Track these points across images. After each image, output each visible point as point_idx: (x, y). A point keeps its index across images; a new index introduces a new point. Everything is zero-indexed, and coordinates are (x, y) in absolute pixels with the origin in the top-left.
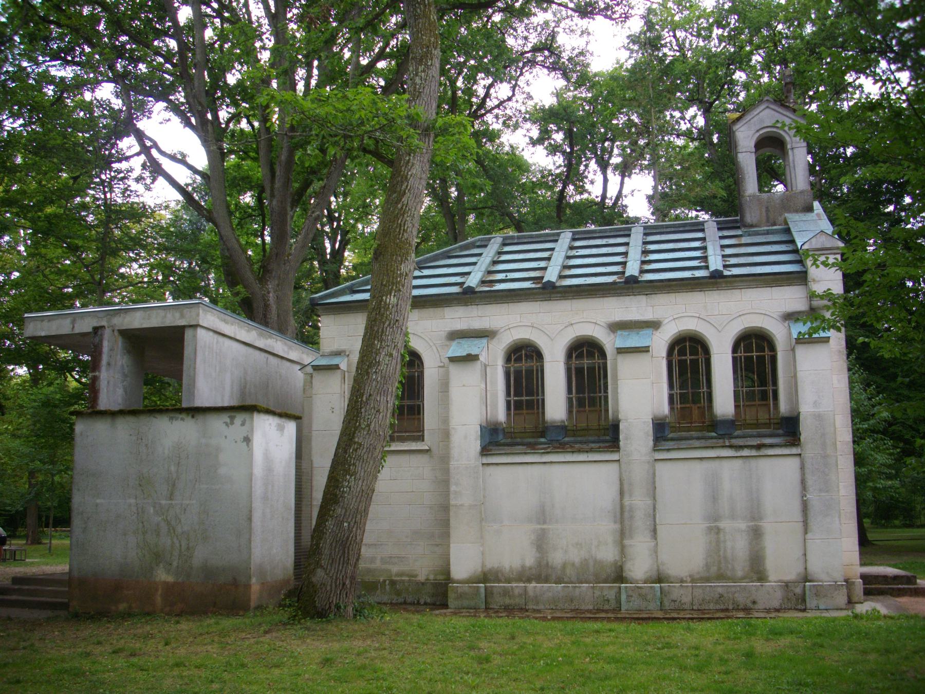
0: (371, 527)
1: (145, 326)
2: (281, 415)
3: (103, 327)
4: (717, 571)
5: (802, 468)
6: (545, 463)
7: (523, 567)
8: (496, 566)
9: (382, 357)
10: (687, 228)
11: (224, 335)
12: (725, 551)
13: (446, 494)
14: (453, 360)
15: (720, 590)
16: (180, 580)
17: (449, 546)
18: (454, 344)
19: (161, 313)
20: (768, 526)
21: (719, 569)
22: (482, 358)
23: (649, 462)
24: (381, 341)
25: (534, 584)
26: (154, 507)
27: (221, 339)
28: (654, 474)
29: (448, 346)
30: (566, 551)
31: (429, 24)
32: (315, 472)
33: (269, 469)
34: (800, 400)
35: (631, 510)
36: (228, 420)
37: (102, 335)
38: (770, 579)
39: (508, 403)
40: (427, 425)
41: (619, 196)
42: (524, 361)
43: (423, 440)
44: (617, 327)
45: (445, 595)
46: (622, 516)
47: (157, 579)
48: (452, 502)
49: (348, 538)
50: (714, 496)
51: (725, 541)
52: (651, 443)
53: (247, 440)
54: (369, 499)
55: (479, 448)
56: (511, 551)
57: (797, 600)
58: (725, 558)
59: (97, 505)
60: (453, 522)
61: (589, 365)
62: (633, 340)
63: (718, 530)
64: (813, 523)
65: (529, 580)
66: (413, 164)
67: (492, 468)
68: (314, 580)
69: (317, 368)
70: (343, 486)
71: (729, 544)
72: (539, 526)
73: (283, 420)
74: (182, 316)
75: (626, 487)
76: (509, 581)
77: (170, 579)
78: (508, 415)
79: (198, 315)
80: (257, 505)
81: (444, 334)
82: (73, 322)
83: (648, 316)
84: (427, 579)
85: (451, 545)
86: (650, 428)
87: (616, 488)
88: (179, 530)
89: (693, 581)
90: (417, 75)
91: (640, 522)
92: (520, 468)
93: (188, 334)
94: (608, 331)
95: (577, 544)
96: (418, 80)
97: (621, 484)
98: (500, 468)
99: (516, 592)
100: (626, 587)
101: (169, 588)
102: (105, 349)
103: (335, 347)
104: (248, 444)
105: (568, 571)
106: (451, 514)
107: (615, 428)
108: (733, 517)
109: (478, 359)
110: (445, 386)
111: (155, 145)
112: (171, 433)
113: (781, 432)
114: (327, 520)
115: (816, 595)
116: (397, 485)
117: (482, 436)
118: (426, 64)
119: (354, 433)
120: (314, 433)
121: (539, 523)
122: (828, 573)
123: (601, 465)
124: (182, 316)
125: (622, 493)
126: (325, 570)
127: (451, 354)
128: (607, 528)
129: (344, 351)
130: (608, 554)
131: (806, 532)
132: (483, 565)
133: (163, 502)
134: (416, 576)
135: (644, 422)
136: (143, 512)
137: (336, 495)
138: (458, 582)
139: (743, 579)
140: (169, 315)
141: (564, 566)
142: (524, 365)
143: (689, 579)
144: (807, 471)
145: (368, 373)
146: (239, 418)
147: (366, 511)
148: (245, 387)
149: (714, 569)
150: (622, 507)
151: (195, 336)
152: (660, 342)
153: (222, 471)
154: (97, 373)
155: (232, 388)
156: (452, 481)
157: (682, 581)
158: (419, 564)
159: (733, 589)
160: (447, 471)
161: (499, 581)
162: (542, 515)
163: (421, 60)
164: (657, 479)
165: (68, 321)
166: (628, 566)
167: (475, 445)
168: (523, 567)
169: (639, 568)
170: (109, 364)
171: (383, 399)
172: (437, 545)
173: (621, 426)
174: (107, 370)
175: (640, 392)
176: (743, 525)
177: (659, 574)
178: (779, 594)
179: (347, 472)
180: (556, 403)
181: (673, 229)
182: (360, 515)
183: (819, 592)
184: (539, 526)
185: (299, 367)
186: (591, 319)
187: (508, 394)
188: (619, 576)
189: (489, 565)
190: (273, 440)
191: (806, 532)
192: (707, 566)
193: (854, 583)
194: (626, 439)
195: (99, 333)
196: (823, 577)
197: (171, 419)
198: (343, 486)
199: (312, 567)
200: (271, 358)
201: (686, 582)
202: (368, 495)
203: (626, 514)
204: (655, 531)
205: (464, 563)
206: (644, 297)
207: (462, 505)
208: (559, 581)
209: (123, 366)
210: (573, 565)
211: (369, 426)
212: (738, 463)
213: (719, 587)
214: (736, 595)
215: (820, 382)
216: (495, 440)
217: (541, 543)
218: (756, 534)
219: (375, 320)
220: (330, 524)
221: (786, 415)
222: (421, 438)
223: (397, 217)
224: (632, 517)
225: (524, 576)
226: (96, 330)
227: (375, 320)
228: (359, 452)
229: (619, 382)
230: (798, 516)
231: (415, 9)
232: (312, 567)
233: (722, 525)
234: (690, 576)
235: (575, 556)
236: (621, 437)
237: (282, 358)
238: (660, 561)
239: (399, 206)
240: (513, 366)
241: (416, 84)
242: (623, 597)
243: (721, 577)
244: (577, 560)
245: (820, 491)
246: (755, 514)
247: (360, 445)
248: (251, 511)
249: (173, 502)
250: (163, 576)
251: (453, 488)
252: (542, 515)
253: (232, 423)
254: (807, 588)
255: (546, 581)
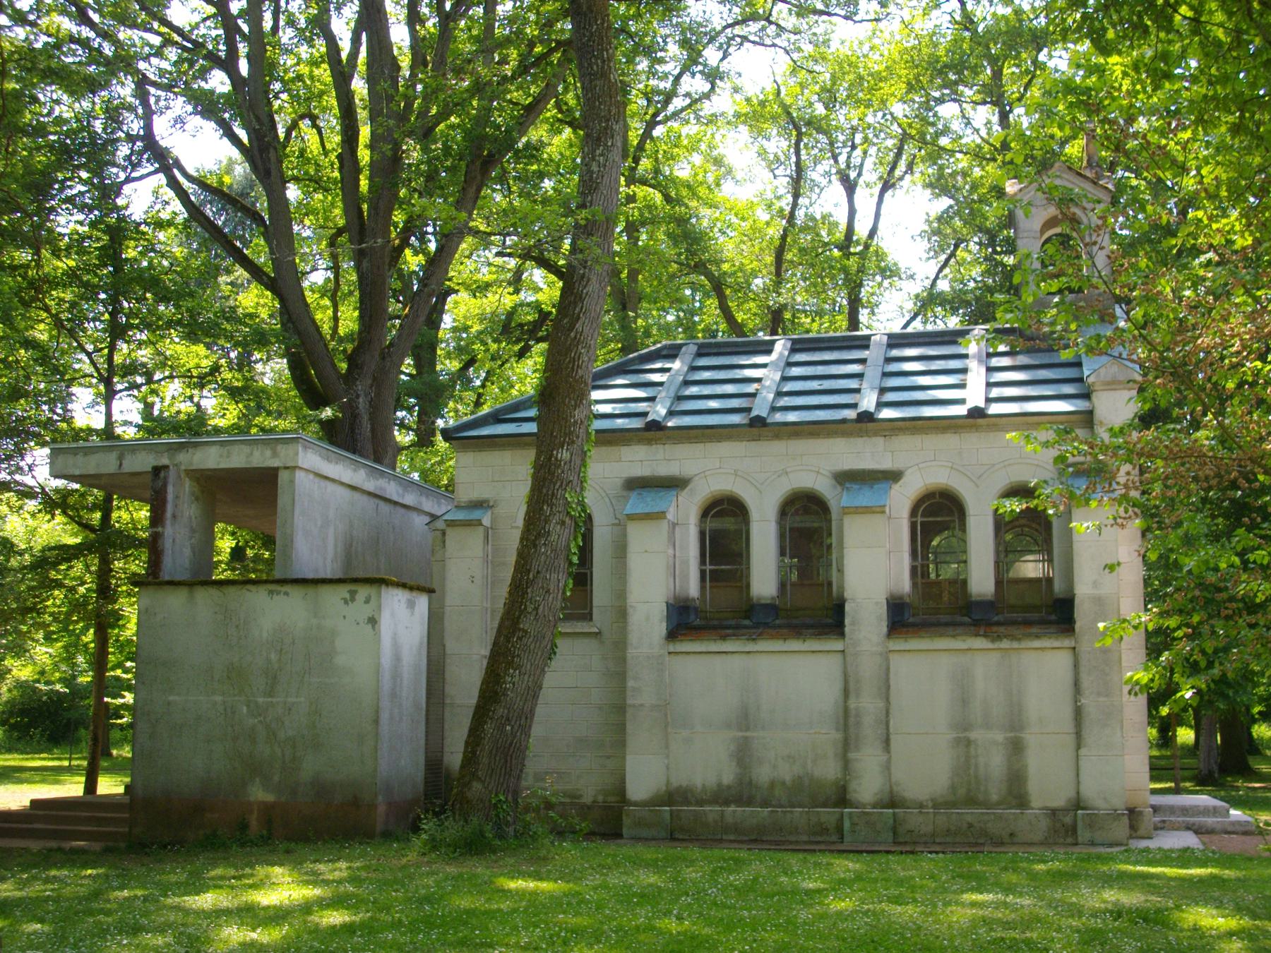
0: (537, 730)
1: (222, 466)
2: (411, 589)
3: (166, 467)
4: (966, 795)
5: (1076, 665)
6: (749, 652)
7: (720, 785)
8: (684, 784)
9: (553, 527)
10: (946, 339)
11: (326, 478)
12: (976, 766)
13: (622, 690)
14: (631, 517)
15: (969, 819)
16: (283, 799)
17: (624, 758)
18: (634, 496)
19: (246, 449)
20: (1031, 739)
21: (969, 791)
22: (670, 516)
23: (881, 654)
24: (551, 506)
25: (732, 808)
26: (248, 706)
27: (324, 483)
28: (888, 669)
29: (627, 499)
30: (773, 767)
31: (609, 88)
32: (448, 661)
33: (397, 658)
34: (1076, 580)
35: (857, 715)
36: (348, 596)
37: (166, 478)
38: (1033, 804)
39: (703, 573)
40: (597, 601)
41: (873, 233)
42: (724, 523)
43: (591, 619)
44: (847, 478)
45: (619, 818)
46: (846, 720)
47: (252, 799)
48: (629, 702)
49: (511, 744)
50: (963, 698)
51: (977, 756)
52: (885, 630)
53: (373, 621)
54: (535, 697)
55: (664, 632)
56: (704, 763)
57: (1067, 831)
58: (976, 777)
59: (169, 703)
60: (629, 727)
61: (808, 523)
62: (864, 497)
63: (969, 743)
64: (1090, 735)
65: (727, 803)
66: (589, 280)
67: (680, 658)
68: (469, 795)
69: (452, 524)
70: (505, 682)
71: (981, 760)
72: (741, 734)
73: (415, 594)
74: (275, 454)
75: (852, 686)
76: (700, 803)
77: (270, 798)
78: (703, 588)
79: (297, 454)
80: (385, 703)
81: (619, 482)
82: (121, 458)
83: (886, 464)
84: (594, 802)
85: (628, 757)
86: (883, 610)
87: (839, 685)
88: (282, 735)
89: (934, 807)
90: (593, 159)
91: (869, 729)
92: (718, 658)
93: (283, 476)
94: (834, 482)
95: (789, 757)
96: (595, 168)
97: (846, 682)
98: (692, 657)
99: (711, 818)
100: (850, 813)
101: (267, 809)
102: (170, 497)
103: (476, 495)
104: (373, 627)
105: (777, 793)
106: (628, 715)
107: (838, 609)
108: (987, 726)
109: (665, 518)
110: (621, 550)
111: (177, 164)
112: (275, 612)
113: (1053, 617)
114: (486, 722)
115: (1091, 826)
116: (567, 681)
117: (669, 617)
118: (606, 145)
119: (519, 617)
120: (447, 609)
121: (741, 730)
122: (1105, 799)
123: (820, 655)
124: (275, 454)
125: (846, 693)
126: (483, 782)
127: (629, 509)
128: (828, 736)
129: (486, 501)
130: (829, 770)
131: (1079, 747)
132: (668, 782)
133: (260, 700)
134: (581, 796)
135: (877, 603)
136: (234, 713)
137: (496, 693)
138: (635, 804)
139: (998, 804)
140: (257, 454)
141: (772, 784)
142: (728, 524)
143: (930, 804)
144: (1082, 669)
145: (535, 546)
146: (363, 591)
147: (532, 712)
148: (351, 546)
149: (962, 792)
150: (846, 711)
151: (292, 481)
152: (901, 498)
153: (340, 660)
154: (160, 529)
155: (336, 546)
156: (630, 674)
157: (921, 806)
158: (588, 783)
159: (986, 817)
160: (623, 661)
161: (688, 803)
162: (745, 719)
163: (599, 139)
164: (892, 676)
165: (113, 457)
166: (853, 786)
167: (661, 629)
168: (720, 785)
169: (867, 788)
170: (174, 516)
171: (554, 576)
172: (608, 757)
173: (847, 607)
174: (173, 525)
175: (873, 563)
176: (1000, 737)
177: (891, 792)
178: (1044, 824)
179: (510, 664)
180: (765, 575)
181: (927, 340)
182: (526, 718)
183: (1093, 822)
184: (741, 734)
185: (427, 519)
186: (812, 465)
187: (703, 562)
188: (841, 797)
189: (675, 783)
190: (401, 620)
191: (1078, 747)
192: (953, 788)
193: (1141, 813)
194: (853, 624)
195: (162, 475)
196: (1099, 803)
197: (271, 592)
198: (505, 682)
199: (467, 779)
200: (382, 504)
201: (926, 807)
202: (534, 692)
203: (852, 720)
204: (887, 742)
205: (644, 777)
206: (880, 441)
207: (642, 705)
208: (765, 804)
209: (190, 517)
210: (783, 783)
211: (536, 609)
212: (997, 655)
213: (971, 814)
214: (989, 825)
215: (1107, 555)
216: (685, 621)
217: (743, 754)
218: (1016, 748)
219: (544, 479)
220: (489, 727)
221: (1061, 596)
222: (588, 617)
223: (569, 350)
224: (858, 724)
225: (722, 796)
226: (157, 470)
227: (544, 479)
228: (524, 640)
229: (845, 551)
230: (1069, 726)
231: (590, 65)
232: (467, 779)
233: (973, 735)
234: (932, 800)
235: (786, 773)
236: (847, 621)
237: (396, 503)
238: (893, 780)
239: (572, 334)
240: (710, 524)
241: (592, 172)
242: (847, 824)
243: (971, 801)
244: (788, 778)
245: (1099, 694)
246: (1015, 723)
247: (526, 632)
248: (377, 712)
249: (274, 700)
250: (259, 794)
251: (630, 683)
252: (745, 719)
253: (353, 599)
254: (1079, 817)
255: (750, 802)
